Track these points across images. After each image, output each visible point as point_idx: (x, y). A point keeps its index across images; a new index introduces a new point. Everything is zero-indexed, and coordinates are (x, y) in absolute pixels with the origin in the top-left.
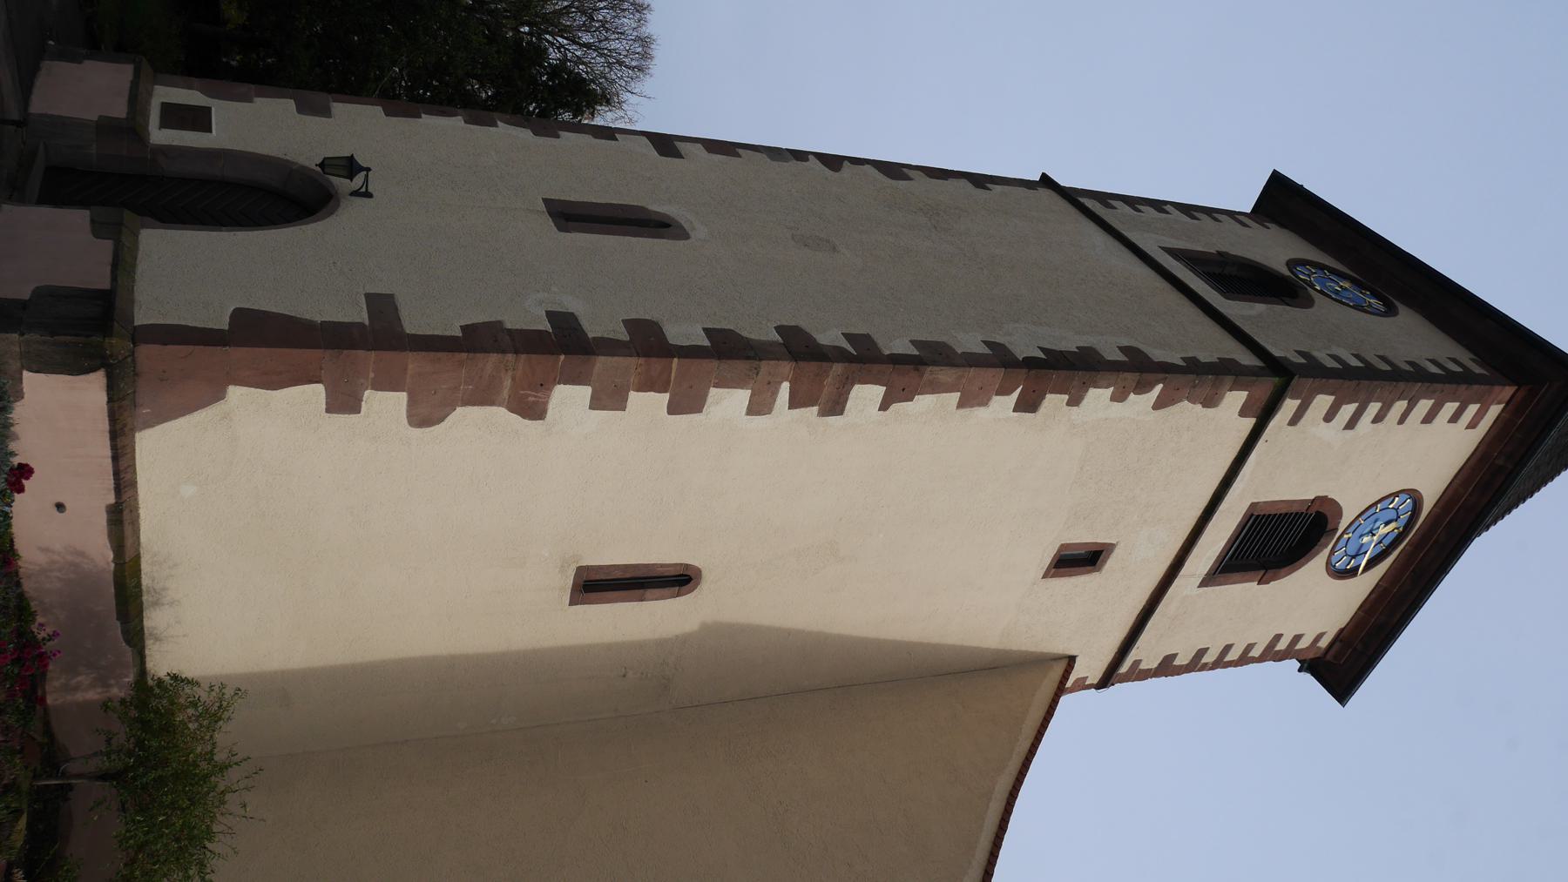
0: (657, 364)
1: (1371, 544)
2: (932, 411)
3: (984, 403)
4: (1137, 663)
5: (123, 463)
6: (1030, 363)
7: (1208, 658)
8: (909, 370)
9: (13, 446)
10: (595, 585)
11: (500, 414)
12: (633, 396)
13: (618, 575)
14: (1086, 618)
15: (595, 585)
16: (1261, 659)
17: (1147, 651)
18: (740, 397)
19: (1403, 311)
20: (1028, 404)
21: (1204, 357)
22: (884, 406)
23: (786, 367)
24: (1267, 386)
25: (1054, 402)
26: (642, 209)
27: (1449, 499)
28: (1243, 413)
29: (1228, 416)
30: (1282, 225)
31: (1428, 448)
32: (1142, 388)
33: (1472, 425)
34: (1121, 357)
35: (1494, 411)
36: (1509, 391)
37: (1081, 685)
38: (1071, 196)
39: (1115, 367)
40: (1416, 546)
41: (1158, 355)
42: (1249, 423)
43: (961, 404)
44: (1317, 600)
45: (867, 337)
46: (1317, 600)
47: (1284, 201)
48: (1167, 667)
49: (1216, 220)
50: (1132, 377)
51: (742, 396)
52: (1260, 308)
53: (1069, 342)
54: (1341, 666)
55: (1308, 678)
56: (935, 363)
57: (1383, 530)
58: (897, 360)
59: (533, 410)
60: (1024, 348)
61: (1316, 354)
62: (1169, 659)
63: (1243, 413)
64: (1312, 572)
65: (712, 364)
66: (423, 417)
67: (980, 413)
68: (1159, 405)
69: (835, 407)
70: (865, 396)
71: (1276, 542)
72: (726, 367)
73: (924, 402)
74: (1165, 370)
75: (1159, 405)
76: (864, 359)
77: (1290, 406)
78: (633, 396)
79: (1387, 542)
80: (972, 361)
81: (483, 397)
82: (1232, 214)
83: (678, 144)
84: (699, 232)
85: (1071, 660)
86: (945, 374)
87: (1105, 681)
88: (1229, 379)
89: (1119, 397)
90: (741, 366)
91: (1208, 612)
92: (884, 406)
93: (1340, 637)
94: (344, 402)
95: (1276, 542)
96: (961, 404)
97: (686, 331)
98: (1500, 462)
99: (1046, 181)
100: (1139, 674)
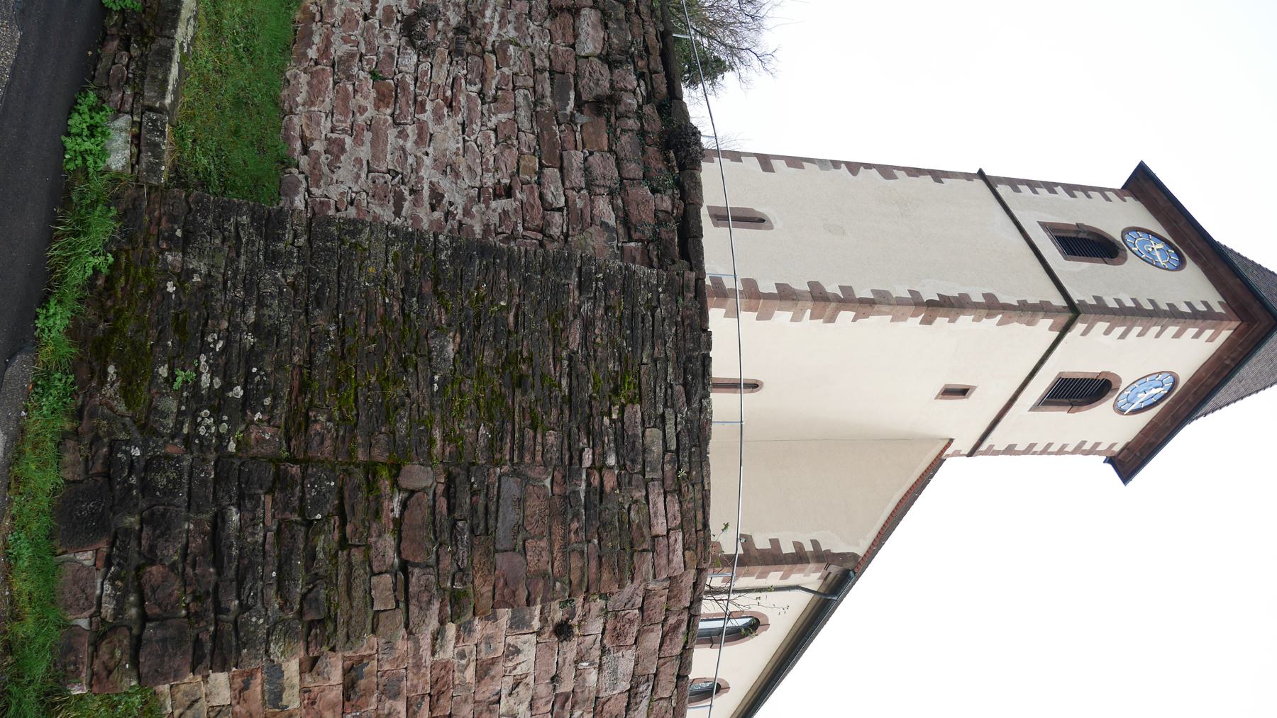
0: (753, 302)
1: (1142, 398)
2: (878, 323)
3: (905, 320)
4: (991, 446)
5: (898, 513)
6: (931, 303)
7: (1053, 449)
8: (866, 306)
14: (963, 421)
16: (1073, 452)
17: (997, 439)
18: (788, 315)
19: (1191, 267)
21: (1031, 301)
22: (854, 320)
24: (1064, 319)
26: (752, 210)
27: (1196, 380)
28: (1051, 329)
29: (1044, 330)
30: (1137, 198)
31: (1188, 352)
33: (1211, 340)
34: (982, 300)
35: (1225, 334)
36: (1235, 324)
37: (957, 454)
39: (977, 306)
40: (1177, 401)
41: (1003, 299)
42: (1055, 334)
43: (892, 321)
44: (1111, 425)
45: (850, 288)
46: (1111, 425)
47: (1143, 184)
48: (1010, 450)
49: (1089, 197)
50: (984, 312)
51: (789, 314)
53: (953, 291)
54: (1127, 463)
55: (1110, 467)
56: (880, 303)
57: (1154, 391)
58: (863, 301)
60: (929, 294)
61: (1105, 298)
62: (1032, 446)
63: (1051, 329)
64: (1104, 409)
65: (777, 302)
67: (901, 324)
68: (1000, 324)
69: (832, 319)
70: (846, 316)
71: (1078, 392)
72: (783, 303)
73: (873, 319)
74: (1006, 308)
75: (1000, 324)
76: (847, 300)
77: (1080, 327)
79: (1154, 400)
80: (901, 302)
82: (1102, 191)
83: (773, 161)
84: (778, 223)
85: (952, 440)
86: (885, 308)
87: (971, 454)
88: (1041, 314)
89: (977, 319)
90: (790, 303)
91: (1029, 423)
92: (854, 320)
93: (1127, 447)
95: (1078, 392)
96: (892, 321)
97: (767, 286)
98: (1228, 362)
99: (981, 174)
100: (991, 452)
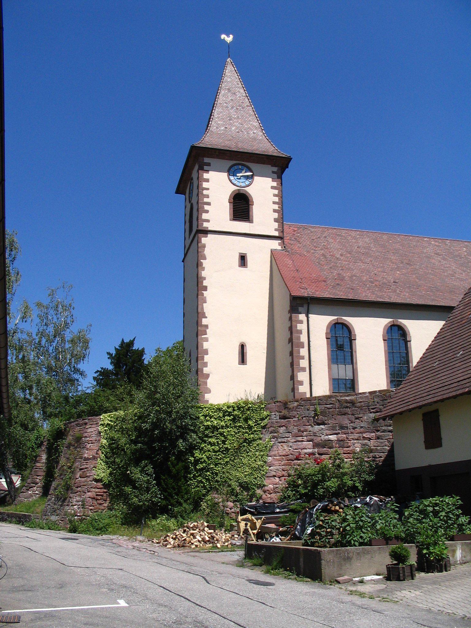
9: (204, 216)
10: (243, 360)
11: (208, 381)
12: (204, 348)
13: (241, 358)
15: (243, 360)
20: (205, 288)
23: (199, 337)
25: (205, 283)
32: (202, 263)
38: (185, 255)
40: (351, 228)
52: (241, 92)
59: (207, 326)
66: (209, 391)
78: (204, 348)
81: (206, 383)
92: (206, 317)
94: (206, 352)
99: (183, 261)
